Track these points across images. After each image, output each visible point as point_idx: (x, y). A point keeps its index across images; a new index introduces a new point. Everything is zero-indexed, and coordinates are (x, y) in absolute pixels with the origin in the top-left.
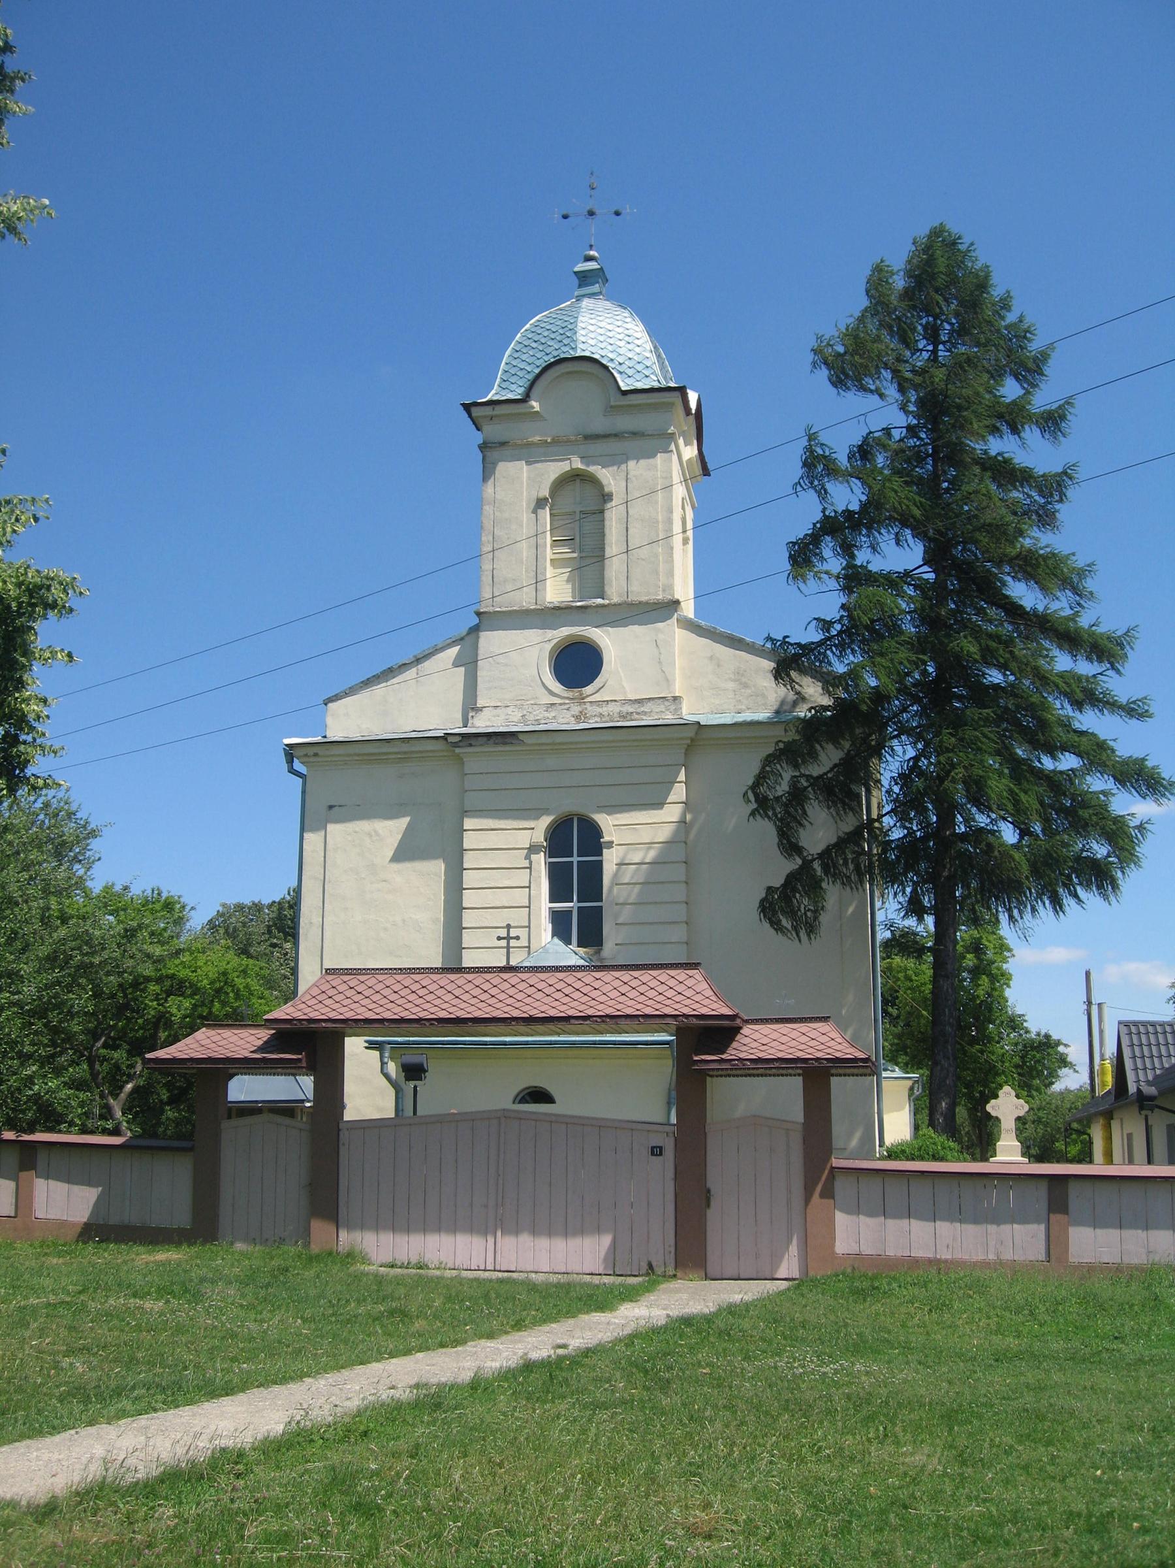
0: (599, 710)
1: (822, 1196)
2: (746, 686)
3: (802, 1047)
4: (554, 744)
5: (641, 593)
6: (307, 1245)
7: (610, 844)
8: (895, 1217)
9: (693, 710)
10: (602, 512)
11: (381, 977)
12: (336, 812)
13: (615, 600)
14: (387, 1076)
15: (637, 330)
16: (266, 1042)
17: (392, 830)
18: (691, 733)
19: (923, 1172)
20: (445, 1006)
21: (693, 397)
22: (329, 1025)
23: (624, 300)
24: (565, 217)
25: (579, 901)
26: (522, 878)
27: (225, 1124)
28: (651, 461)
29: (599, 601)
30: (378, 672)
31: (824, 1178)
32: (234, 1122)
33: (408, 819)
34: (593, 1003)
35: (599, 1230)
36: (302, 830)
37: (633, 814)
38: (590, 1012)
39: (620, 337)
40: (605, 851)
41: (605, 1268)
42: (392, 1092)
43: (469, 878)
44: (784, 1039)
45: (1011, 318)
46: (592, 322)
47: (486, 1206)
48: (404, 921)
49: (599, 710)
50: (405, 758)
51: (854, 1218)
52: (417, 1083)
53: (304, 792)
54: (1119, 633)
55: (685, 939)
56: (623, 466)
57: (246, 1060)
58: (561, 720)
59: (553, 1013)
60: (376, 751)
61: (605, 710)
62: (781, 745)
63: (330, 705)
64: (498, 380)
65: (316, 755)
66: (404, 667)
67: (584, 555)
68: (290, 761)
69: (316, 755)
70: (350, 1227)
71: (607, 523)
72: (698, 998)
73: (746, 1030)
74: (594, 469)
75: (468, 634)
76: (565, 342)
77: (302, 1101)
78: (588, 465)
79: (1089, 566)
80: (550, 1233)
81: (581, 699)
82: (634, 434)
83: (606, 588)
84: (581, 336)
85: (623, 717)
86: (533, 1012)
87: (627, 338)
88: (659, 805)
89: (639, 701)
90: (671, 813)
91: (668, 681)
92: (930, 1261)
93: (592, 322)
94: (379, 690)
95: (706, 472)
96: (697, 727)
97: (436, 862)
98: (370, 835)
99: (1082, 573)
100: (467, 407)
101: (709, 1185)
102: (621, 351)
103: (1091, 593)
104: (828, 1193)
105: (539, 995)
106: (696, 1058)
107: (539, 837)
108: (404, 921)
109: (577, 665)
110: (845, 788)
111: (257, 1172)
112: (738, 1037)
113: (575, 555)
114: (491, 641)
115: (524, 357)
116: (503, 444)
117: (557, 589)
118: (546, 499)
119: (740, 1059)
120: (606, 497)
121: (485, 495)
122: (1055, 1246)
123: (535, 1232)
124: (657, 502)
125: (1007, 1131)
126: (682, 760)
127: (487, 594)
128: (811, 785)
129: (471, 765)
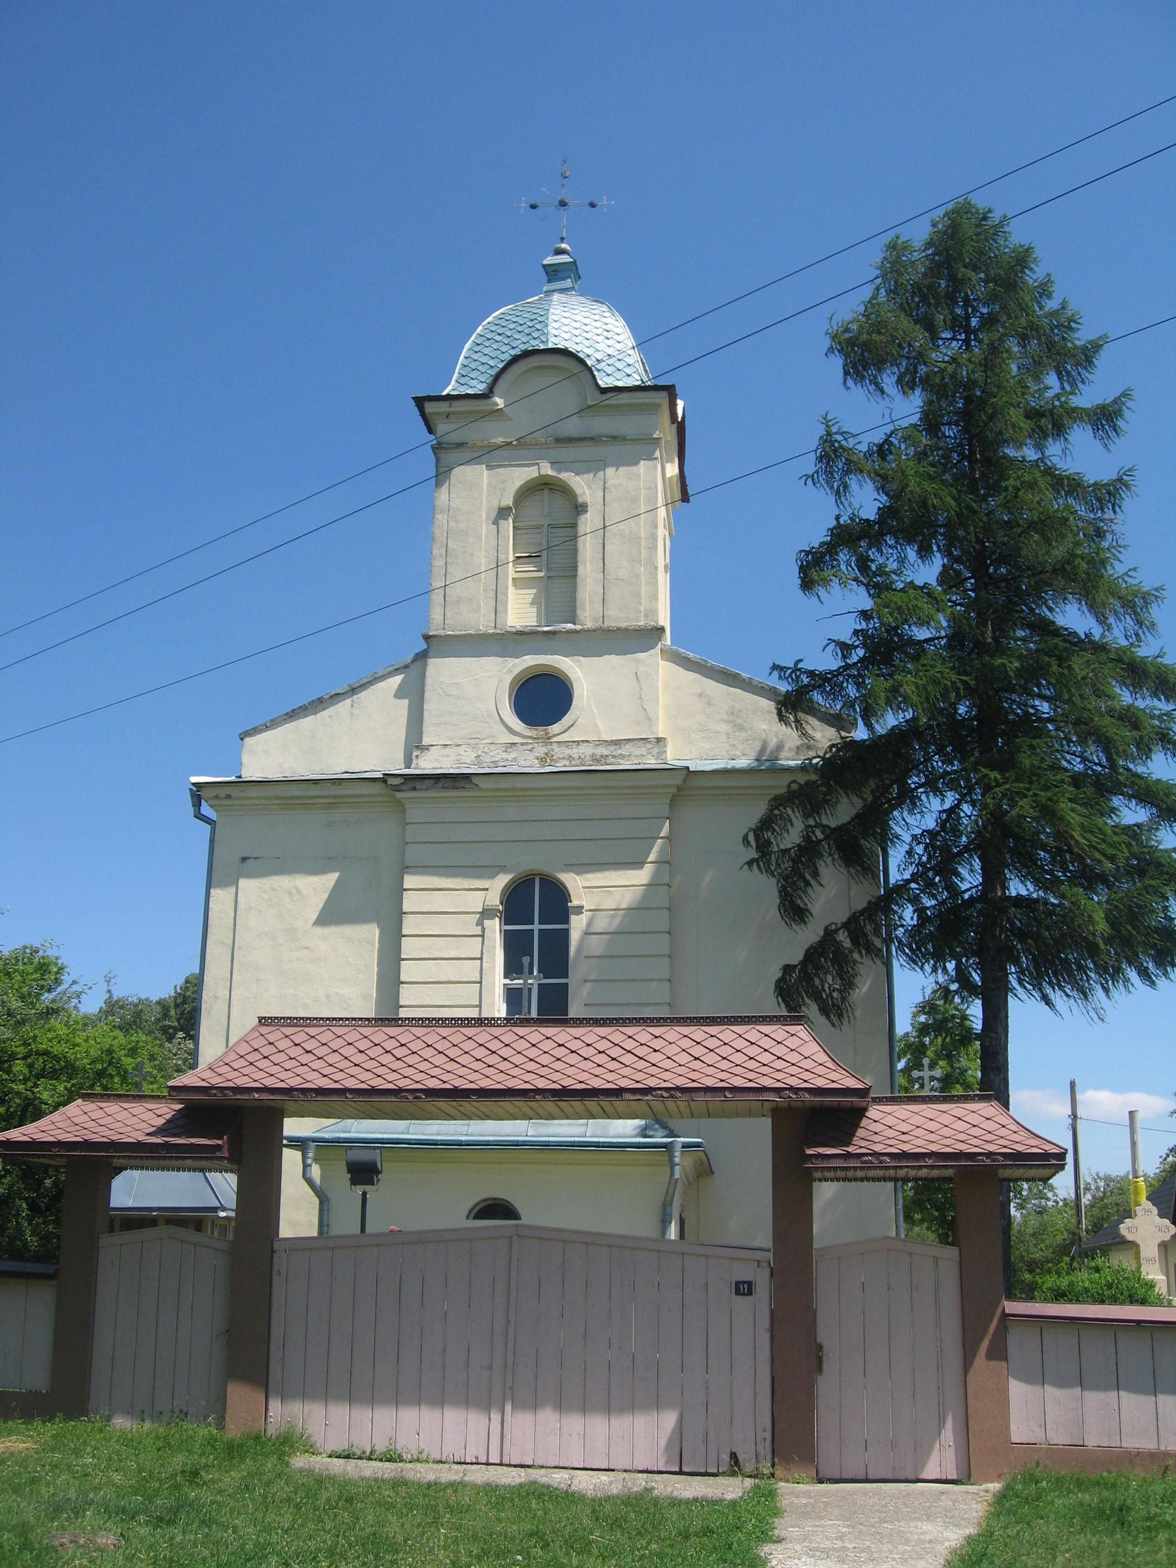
0: (568, 752)
1: (990, 1356)
2: (741, 728)
3: (962, 1137)
4: (515, 789)
5: (618, 618)
6: (221, 1424)
7: (579, 910)
8: (1097, 1388)
9: (681, 753)
10: (574, 526)
11: (339, 1031)
12: (250, 864)
13: (589, 625)
14: (310, 1182)
16: (168, 1121)
17: (316, 889)
20: (435, 1072)
21: (680, 404)
22: (265, 1096)
23: (598, 295)
24: (533, 207)
26: (473, 947)
27: (105, 1240)
28: (634, 468)
29: (570, 626)
31: (991, 1330)
32: (120, 1237)
33: (336, 875)
34: (653, 1070)
35: (657, 1403)
36: (209, 886)
37: (607, 874)
38: (652, 1083)
39: (598, 331)
40: (573, 918)
41: (667, 1462)
42: (316, 1200)
43: (409, 947)
44: (931, 1126)
45: (1051, 305)
46: (566, 314)
47: (490, 1368)
48: (328, 996)
49: (568, 752)
50: (334, 803)
51: (1037, 1389)
52: (367, 1188)
53: (212, 841)
56: (600, 474)
57: (138, 1146)
58: (523, 763)
59: (597, 1083)
60: (299, 793)
61: (575, 752)
62: (794, 787)
63: (247, 740)
64: (456, 375)
65: (229, 797)
66: (336, 698)
67: (552, 574)
70: (284, 1397)
72: (808, 1064)
73: (873, 1112)
74: (565, 476)
75: (413, 662)
76: (535, 335)
77: (215, 1209)
78: (559, 471)
79: (1156, 590)
80: (584, 1408)
81: (547, 739)
82: (614, 438)
83: (579, 612)
84: (552, 328)
86: (567, 1082)
87: (605, 334)
88: (639, 864)
89: (617, 743)
90: (642, 876)
91: (650, 720)
92: (1153, 1456)
93: (566, 314)
94: (307, 722)
95: (685, 498)
96: (685, 772)
97: (366, 927)
98: (291, 894)
99: (1148, 598)
100: (420, 402)
102: (599, 347)
103: (1153, 624)
104: (998, 1352)
105: (573, 1058)
106: (809, 1152)
107: (494, 899)
108: (328, 996)
109: (542, 699)
110: (858, 846)
111: (151, 1314)
112: (864, 1122)
113: (541, 574)
114: (441, 670)
115: (486, 351)
116: (461, 445)
117: (520, 611)
118: (509, 508)
119: (875, 1154)
120: (580, 509)
121: (438, 503)
123: (561, 1406)
127: (437, 615)
128: (826, 838)
129: (414, 813)
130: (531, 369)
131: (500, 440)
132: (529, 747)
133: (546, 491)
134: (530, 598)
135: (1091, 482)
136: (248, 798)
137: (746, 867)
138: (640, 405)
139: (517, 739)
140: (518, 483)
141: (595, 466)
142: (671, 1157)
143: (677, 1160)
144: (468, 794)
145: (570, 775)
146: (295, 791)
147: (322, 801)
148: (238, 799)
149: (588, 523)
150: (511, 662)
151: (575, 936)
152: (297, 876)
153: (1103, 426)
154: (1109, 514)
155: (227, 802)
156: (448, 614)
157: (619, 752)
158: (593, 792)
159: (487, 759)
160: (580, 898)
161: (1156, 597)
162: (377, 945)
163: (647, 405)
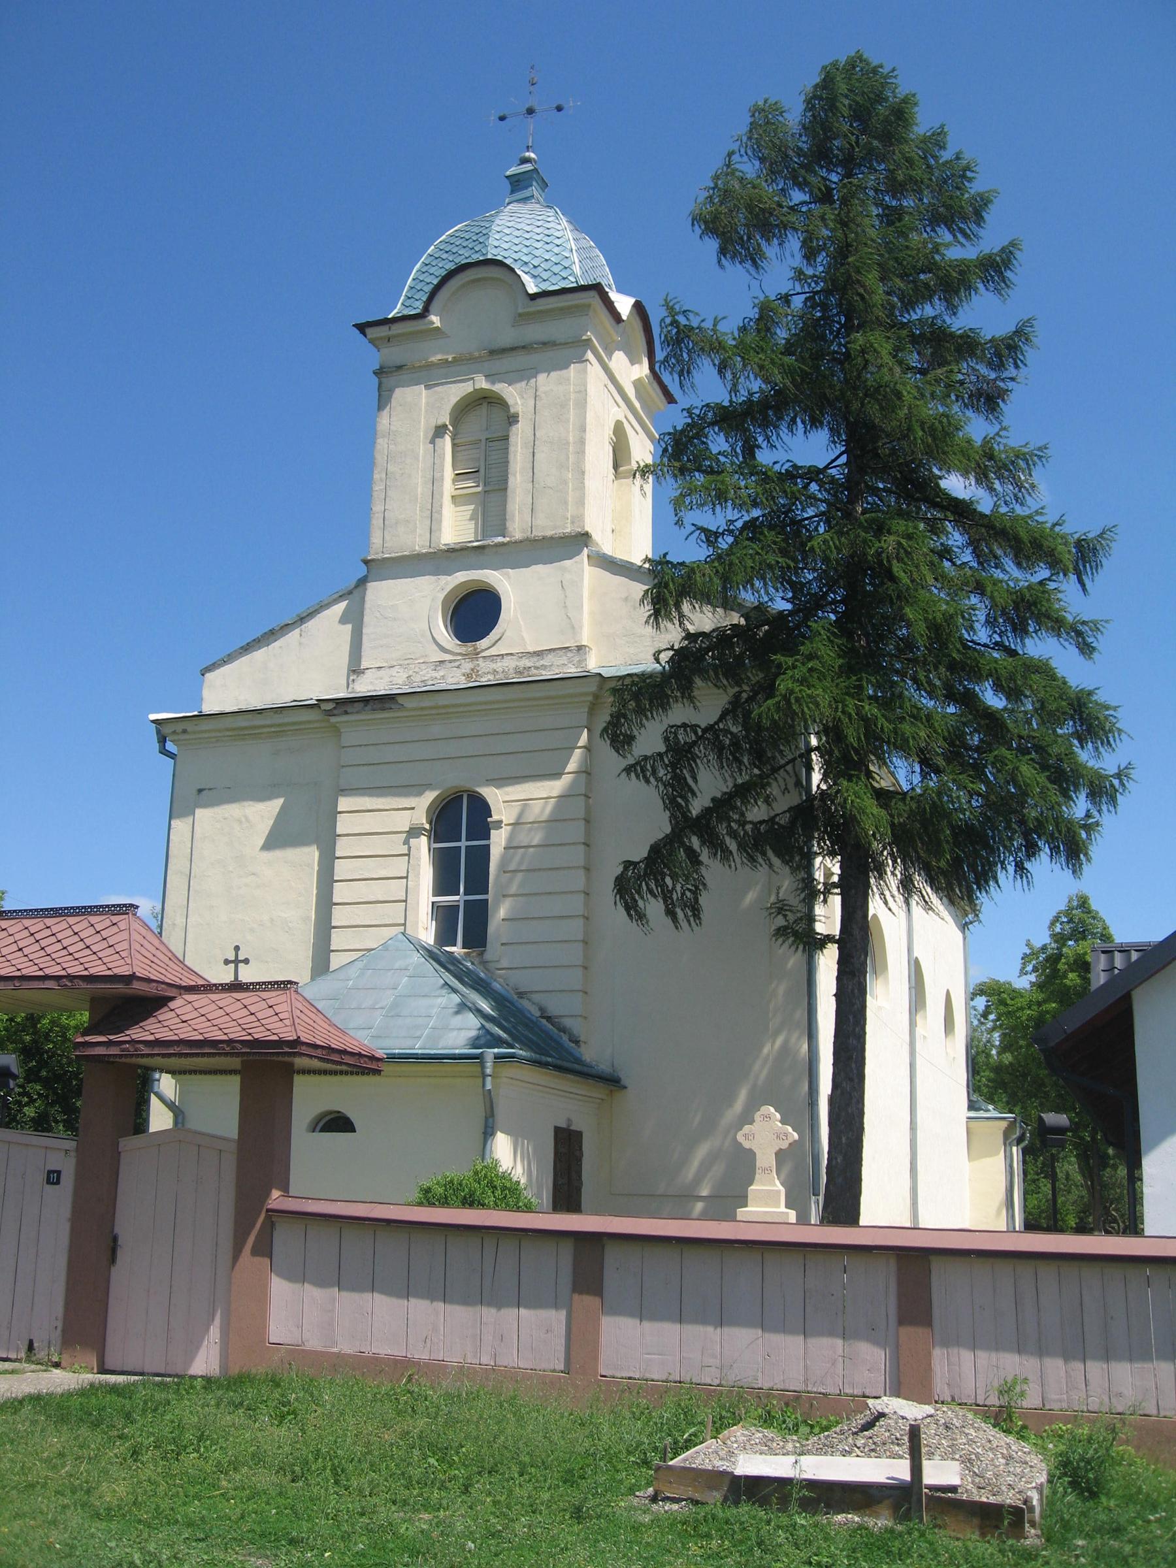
0: (494, 666)
5: (546, 527)
10: (506, 438)
13: (518, 536)
15: (561, 227)
17: (262, 814)
18: (592, 687)
19: (389, 1222)
24: (502, 119)
25: (466, 894)
28: (564, 371)
29: (500, 539)
30: (259, 635)
33: (281, 801)
39: (538, 238)
43: (342, 869)
45: (946, 155)
48: (272, 920)
49: (494, 666)
50: (279, 732)
51: (297, 1286)
54: (1090, 536)
55: (580, 937)
61: (499, 665)
63: (207, 675)
65: (185, 731)
66: (286, 628)
68: (162, 740)
69: (185, 731)
71: (512, 449)
78: (493, 383)
79: (1040, 449)
82: (544, 344)
85: (519, 672)
88: (557, 775)
89: (539, 654)
91: (574, 628)
94: (259, 655)
97: (306, 850)
98: (240, 822)
101: (117, 1230)
102: (537, 253)
104: (264, 1249)
107: (421, 818)
108: (272, 920)
109: (474, 614)
113: (479, 489)
114: (380, 593)
116: (400, 368)
117: (456, 527)
118: (445, 426)
120: (513, 419)
122: (580, 1345)
124: (568, 420)
125: (764, 1170)
126: (583, 719)
127: (376, 539)
130: (463, 286)
131: (435, 358)
132: (457, 664)
133: (485, 404)
134: (468, 514)
135: (989, 337)
136: (202, 732)
137: (624, 774)
138: (569, 308)
139: (448, 657)
140: (454, 400)
141: (526, 374)
142: (483, 1067)
143: (488, 1071)
144: (396, 714)
145: (524, 686)
146: (242, 722)
147: (268, 730)
148: (194, 733)
149: (519, 435)
150: (444, 579)
151: (496, 852)
152: (246, 804)
153: (992, 277)
154: (1011, 371)
155: (186, 736)
156: (387, 537)
157: (542, 662)
158: (522, 704)
159: (417, 678)
160: (500, 813)
161: (1040, 457)
162: (316, 868)
163: (577, 306)
